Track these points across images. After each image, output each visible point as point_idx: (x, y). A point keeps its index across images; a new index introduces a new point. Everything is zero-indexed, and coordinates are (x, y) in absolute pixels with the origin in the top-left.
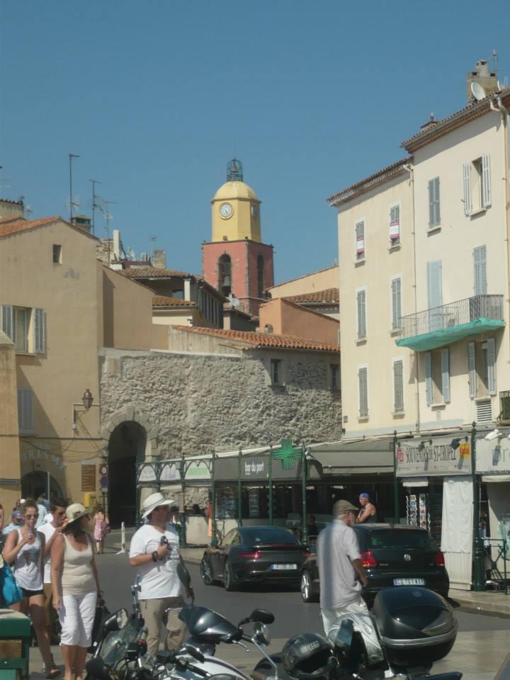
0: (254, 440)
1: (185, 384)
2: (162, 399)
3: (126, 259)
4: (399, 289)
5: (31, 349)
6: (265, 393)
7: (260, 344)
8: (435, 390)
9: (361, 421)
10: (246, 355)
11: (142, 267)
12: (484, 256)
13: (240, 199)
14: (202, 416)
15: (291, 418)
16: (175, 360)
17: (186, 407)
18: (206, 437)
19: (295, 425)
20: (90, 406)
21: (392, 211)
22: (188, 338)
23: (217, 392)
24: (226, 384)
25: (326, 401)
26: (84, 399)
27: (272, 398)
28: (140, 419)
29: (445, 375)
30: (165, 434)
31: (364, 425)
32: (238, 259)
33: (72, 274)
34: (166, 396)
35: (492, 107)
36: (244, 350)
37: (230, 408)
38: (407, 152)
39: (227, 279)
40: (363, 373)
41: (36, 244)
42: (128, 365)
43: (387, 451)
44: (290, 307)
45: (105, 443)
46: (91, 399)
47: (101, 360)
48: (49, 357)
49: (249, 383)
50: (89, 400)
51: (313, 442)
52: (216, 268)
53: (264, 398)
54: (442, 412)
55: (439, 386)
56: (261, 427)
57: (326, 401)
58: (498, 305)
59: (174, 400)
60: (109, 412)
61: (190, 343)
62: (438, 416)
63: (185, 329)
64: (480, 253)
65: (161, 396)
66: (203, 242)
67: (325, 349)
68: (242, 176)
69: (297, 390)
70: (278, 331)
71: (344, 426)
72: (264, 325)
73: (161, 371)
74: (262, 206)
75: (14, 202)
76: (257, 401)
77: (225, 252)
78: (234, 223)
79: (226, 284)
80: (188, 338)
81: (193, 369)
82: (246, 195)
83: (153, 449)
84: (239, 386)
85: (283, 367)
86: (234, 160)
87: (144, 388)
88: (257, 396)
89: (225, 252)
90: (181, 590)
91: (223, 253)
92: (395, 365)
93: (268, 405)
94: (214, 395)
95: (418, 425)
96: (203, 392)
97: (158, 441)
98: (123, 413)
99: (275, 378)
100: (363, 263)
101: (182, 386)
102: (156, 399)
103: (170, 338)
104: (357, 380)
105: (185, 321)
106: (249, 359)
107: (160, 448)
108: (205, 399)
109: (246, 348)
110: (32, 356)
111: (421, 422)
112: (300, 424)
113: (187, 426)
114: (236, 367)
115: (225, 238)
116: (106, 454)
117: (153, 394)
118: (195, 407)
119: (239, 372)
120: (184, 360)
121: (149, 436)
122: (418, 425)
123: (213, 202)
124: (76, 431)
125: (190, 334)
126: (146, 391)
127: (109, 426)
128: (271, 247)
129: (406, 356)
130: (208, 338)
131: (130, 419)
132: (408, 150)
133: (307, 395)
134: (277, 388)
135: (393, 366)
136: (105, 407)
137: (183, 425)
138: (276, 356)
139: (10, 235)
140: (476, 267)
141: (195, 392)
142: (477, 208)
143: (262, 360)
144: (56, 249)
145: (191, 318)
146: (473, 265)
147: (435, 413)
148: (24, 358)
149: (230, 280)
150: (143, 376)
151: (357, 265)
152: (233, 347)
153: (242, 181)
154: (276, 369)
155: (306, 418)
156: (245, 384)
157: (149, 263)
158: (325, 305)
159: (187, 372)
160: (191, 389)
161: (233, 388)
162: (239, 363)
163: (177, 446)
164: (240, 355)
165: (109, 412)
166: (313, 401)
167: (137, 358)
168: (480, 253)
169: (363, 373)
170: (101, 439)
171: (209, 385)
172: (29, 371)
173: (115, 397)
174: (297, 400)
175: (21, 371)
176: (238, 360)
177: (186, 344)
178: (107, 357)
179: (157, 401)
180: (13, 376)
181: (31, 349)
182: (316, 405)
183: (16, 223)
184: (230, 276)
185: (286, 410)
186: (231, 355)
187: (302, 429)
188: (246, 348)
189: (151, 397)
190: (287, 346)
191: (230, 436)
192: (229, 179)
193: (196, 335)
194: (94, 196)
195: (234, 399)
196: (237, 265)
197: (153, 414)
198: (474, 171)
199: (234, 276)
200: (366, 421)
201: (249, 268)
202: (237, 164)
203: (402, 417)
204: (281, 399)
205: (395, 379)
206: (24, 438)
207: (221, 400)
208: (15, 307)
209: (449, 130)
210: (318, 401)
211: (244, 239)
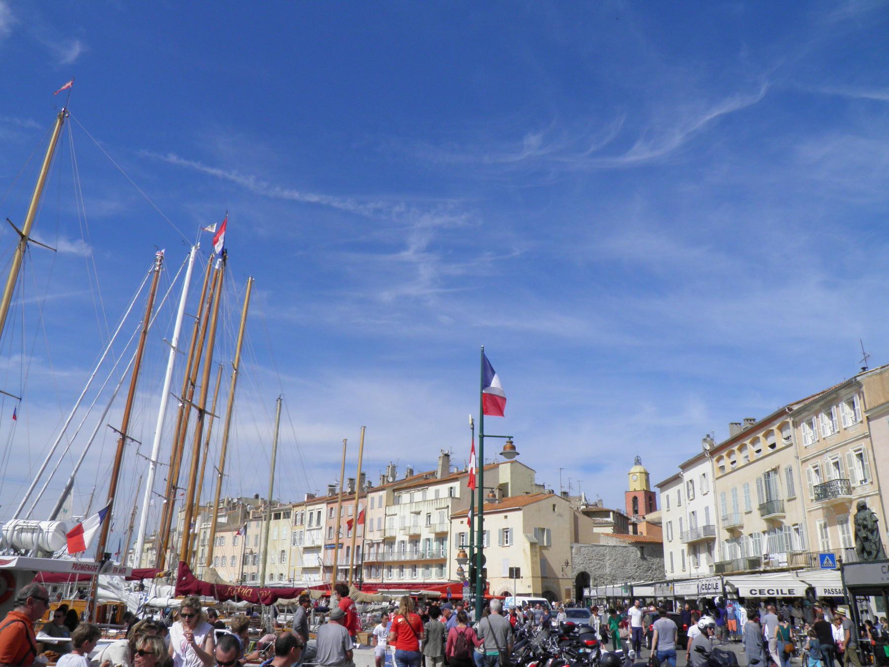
0: (634, 579)
3: (588, 504)
5: (545, 544)
8: (695, 558)
9: (671, 572)
10: (630, 545)
11: (593, 507)
12: (708, 510)
13: (640, 473)
14: (612, 569)
15: (649, 570)
16: (601, 548)
17: (606, 566)
18: (614, 578)
19: (651, 573)
20: (567, 565)
26: (565, 563)
27: (641, 562)
28: (588, 570)
29: (698, 554)
30: (598, 577)
31: (672, 574)
33: (560, 515)
34: (598, 562)
35: (706, 455)
36: (628, 543)
37: (623, 566)
39: (636, 507)
40: (671, 553)
41: (548, 503)
42: (582, 550)
43: (442, 571)
44: (650, 524)
45: (574, 580)
46: (568, 563)
47: (572, 548)
48: (552, 546)
50: (567, 564)
51: (659, 580)
52: (632, 502)
54: (698, 569)
55: (696, 556)
56: (637, 574)
58: (713, 529)
60: (575, 568)
62: (697, 571)
63: (607, 535)
69: (651, 559)
70: (645, 534)
71: (666, 574)
74: (650, 475)
75: (540, 485)
78: (638, 482)
79: (636, 509)
82: (643, 471)
83: (593, 582)
85: (645, 550)
86: (638, 457)
94: (617, 561)
95: (690, 574)
96: (612, 560)
97: (595, 579)
98: (580, 568)
99: (642, 554)
100: (669, 510)
103: (600, 538)
105: (609, 530)
107: (596, 582)
110: (545, 547)
111: (692, 573)
112: (653, 573)
113: (606, 574)
114: (625, 550)
115: (635, 489)
116: (575, 584)
117: (592, 561)
118: (609, 566)
120: (604, 547)
121: (591, 577)
122: (690, 574)
123: (629, 474)
124: (563, 575)
126: (589, 560)
127: (575, 573)
128: (655, 493)
129: (685, 547)
130: (615, 538)
131: (583, 570)
134: (643, 558)
136: (574, 566)
137: (605, 573)
138: (642, 545)
139: (537, 501)
140: (706, 514)
142: (705, 492)
143: (636, 547)
144: (554, 506)
145: (612, 528)
146: (705, 513)
147: (696, 570)
148: (543, 548)
149: (638, 507)
151: (668, 511)
152: (624, 542)
153: (641, 465)
154: (642, 551)
155: (656, 570)
157: (596, 505)
158: (657, 524)
159: (606, 552)
163: (603, 581)
164: (627, 545)
165: (575, 568)
166: (658, 563)
167: (586, 547)
169: (671, 553)
170: (573, 579)
172: (545, 552)
173: (578, 562)
175: (543, 553)
176: (626, 547)
178: (574, 547)
180: (538, 554)
181: (545, 544)
182: (659, 565)
183: (540, 496)
184: (637, 505)
185: (647, 567)
187: (654, 575)
191: (624, 577)
192: (636, 464)
194: (570, 484)
197: (593, 569)
198: (703, 477)
199: (639, 506)
200: (673, 572)
201: (645, 502)
203: (685, 571)
204: (645, 563)
206: (542, 578)
207: (620, 563)
208: (539, 528)
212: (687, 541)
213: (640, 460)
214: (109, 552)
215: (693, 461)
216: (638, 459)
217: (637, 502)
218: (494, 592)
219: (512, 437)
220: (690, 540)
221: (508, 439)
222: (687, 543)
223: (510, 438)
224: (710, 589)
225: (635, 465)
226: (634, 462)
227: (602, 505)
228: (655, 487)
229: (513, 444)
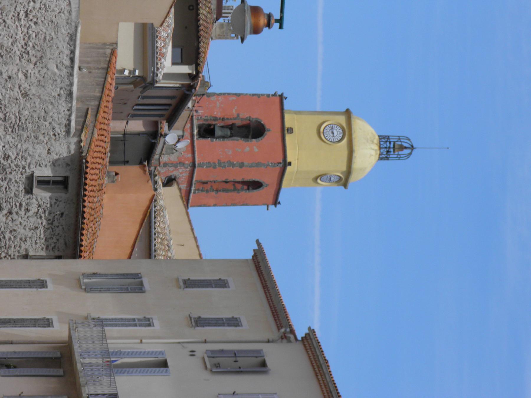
1: (35, 64)
2: (16, 34)
4: (141, 325)
6: (24, 168)
7: (87, 162)
16: (67, 52)
21: (236, 318)
22: (98, 69)
23: (25, 106)
24: (35, 115)
25: (12, 248)
32: (256, 150)
38: (304, 335)
49: (37, 146)
53: (17, 166)
57: (12, 248)
59: (15, 48)
61: (93, 71)
64: (234, 322)
65: (20, 32)
66: (285, 95)
67: (82, 248)
68: (387, 158)
72: (118, 172)
73: (53, 34)
76: (13, 157)
77: (269, 130)
80: (98, 69)
81: (55, 74)
84: (32, 134)
86: (412, 148)
87: (31, 11)
88: (20, 157)
89: (269, 130)
90: (125, 75)
91: (267, 127)
92: (48, 319)
93: (8, 170)
94: (22, 100)
96: (25, 85)
101: (34, 60)
102: (17, 26)
104: (33, 276)
106: (68, 147)
108: (16, 89)
109: (82, 144)
114: (58, 130)
119: (52, 134)
125: (104, 71)
132: (305, 337)
133: (21, 224)
135: (47, 317)
141: (26, 75)
149: (223, 137)
150: (46, 10)
153: (381, 159)
154: (55, 183)
156: (36, 141)
160: (30, 71)
161: (30, 126)
162: (64, 134)
168: (234, 322)
169: (42, 284)
171: (34, 95)
174: (14, 210)
177: (91, 65)
179: (15, 27)
186: (73, 123)
188: (82, 144)
189: (19, 20)
190: (86, 198)
192: (384, 139)
193: (103, 80)
195: (16, 126)
196: (247, 149)
199: (229, 143)
202: (406, 151)
205: (31, 319)
209: (320, 379)
210: (12, 237)
211: (289, 160)
212: (75, 341)
213: (399, 158)
214: (88, 177)
215: (323, 375)
216: (402, 148)
217: (246, 137)
218: (76, 321)
219: (281, 27)
220: (77, 349)
221: (279, 18)
222: (70, 337)
223: (280, 21)
224: (85, 358)
225: (381, 137)
226: (393, 132)
227: (221, 37)
228: (257, 241)
229: (266, 29)
